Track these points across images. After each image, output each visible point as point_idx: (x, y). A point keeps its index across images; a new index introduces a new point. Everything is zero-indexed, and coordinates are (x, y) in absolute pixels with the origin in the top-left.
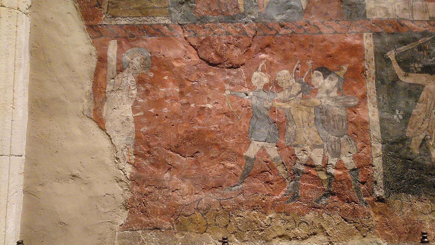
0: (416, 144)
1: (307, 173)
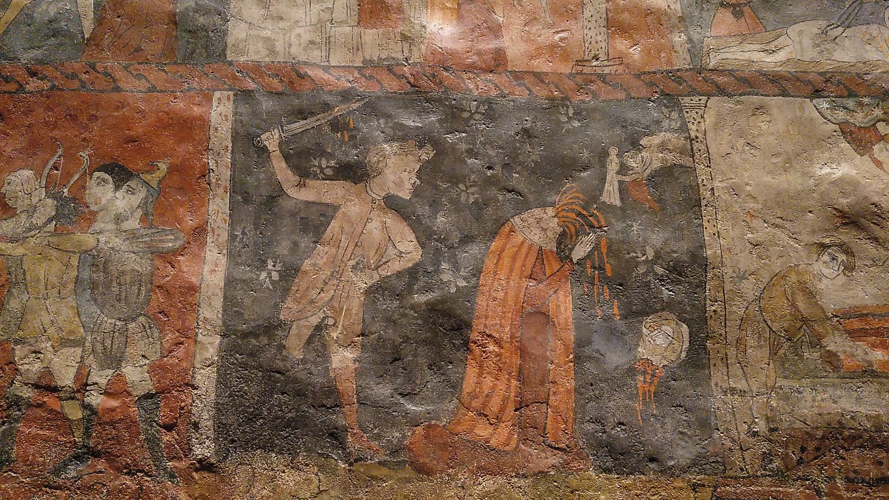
0: (299, 336)
1: (39, 406)
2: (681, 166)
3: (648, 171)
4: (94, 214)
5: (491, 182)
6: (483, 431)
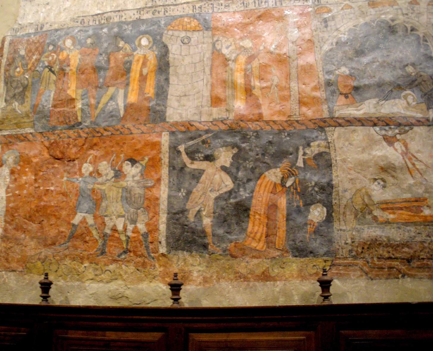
0: (192, 214)
2: (325, 152)
3: (313, 155)
4: (125, 175)
5: (257, 160)
6: (254, 244)
